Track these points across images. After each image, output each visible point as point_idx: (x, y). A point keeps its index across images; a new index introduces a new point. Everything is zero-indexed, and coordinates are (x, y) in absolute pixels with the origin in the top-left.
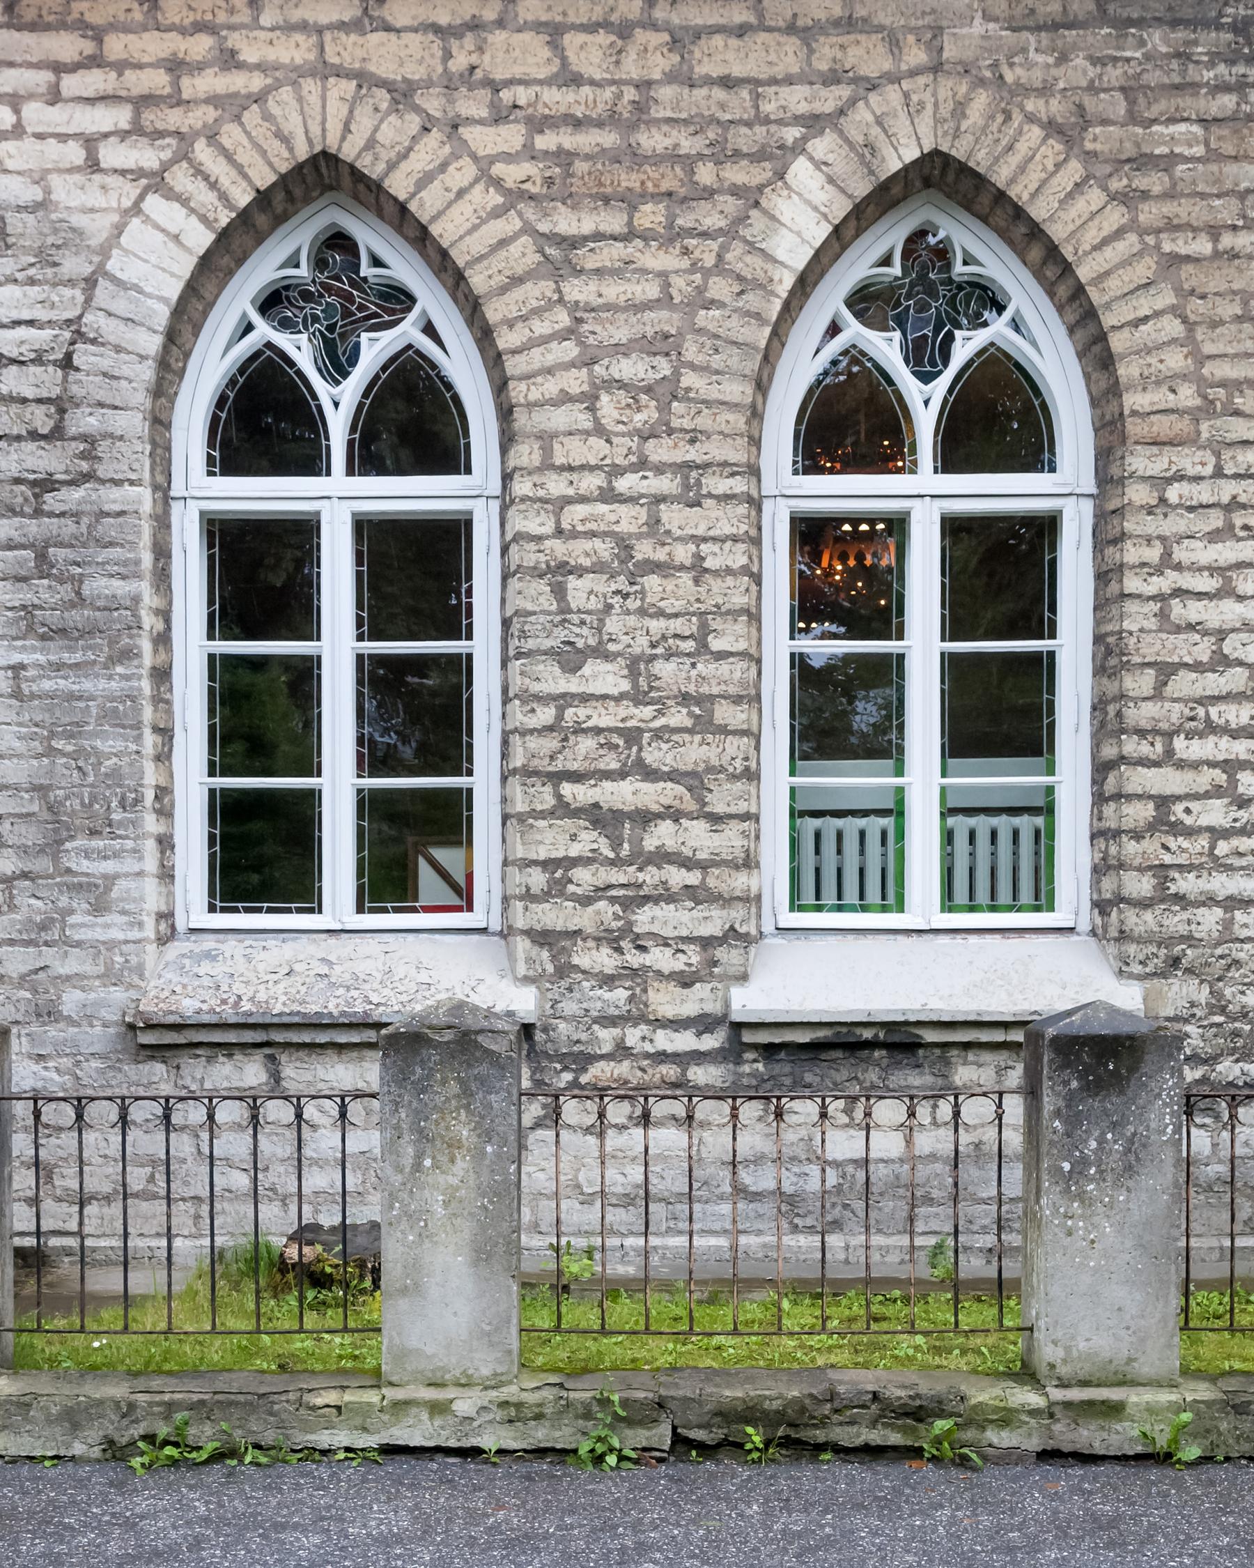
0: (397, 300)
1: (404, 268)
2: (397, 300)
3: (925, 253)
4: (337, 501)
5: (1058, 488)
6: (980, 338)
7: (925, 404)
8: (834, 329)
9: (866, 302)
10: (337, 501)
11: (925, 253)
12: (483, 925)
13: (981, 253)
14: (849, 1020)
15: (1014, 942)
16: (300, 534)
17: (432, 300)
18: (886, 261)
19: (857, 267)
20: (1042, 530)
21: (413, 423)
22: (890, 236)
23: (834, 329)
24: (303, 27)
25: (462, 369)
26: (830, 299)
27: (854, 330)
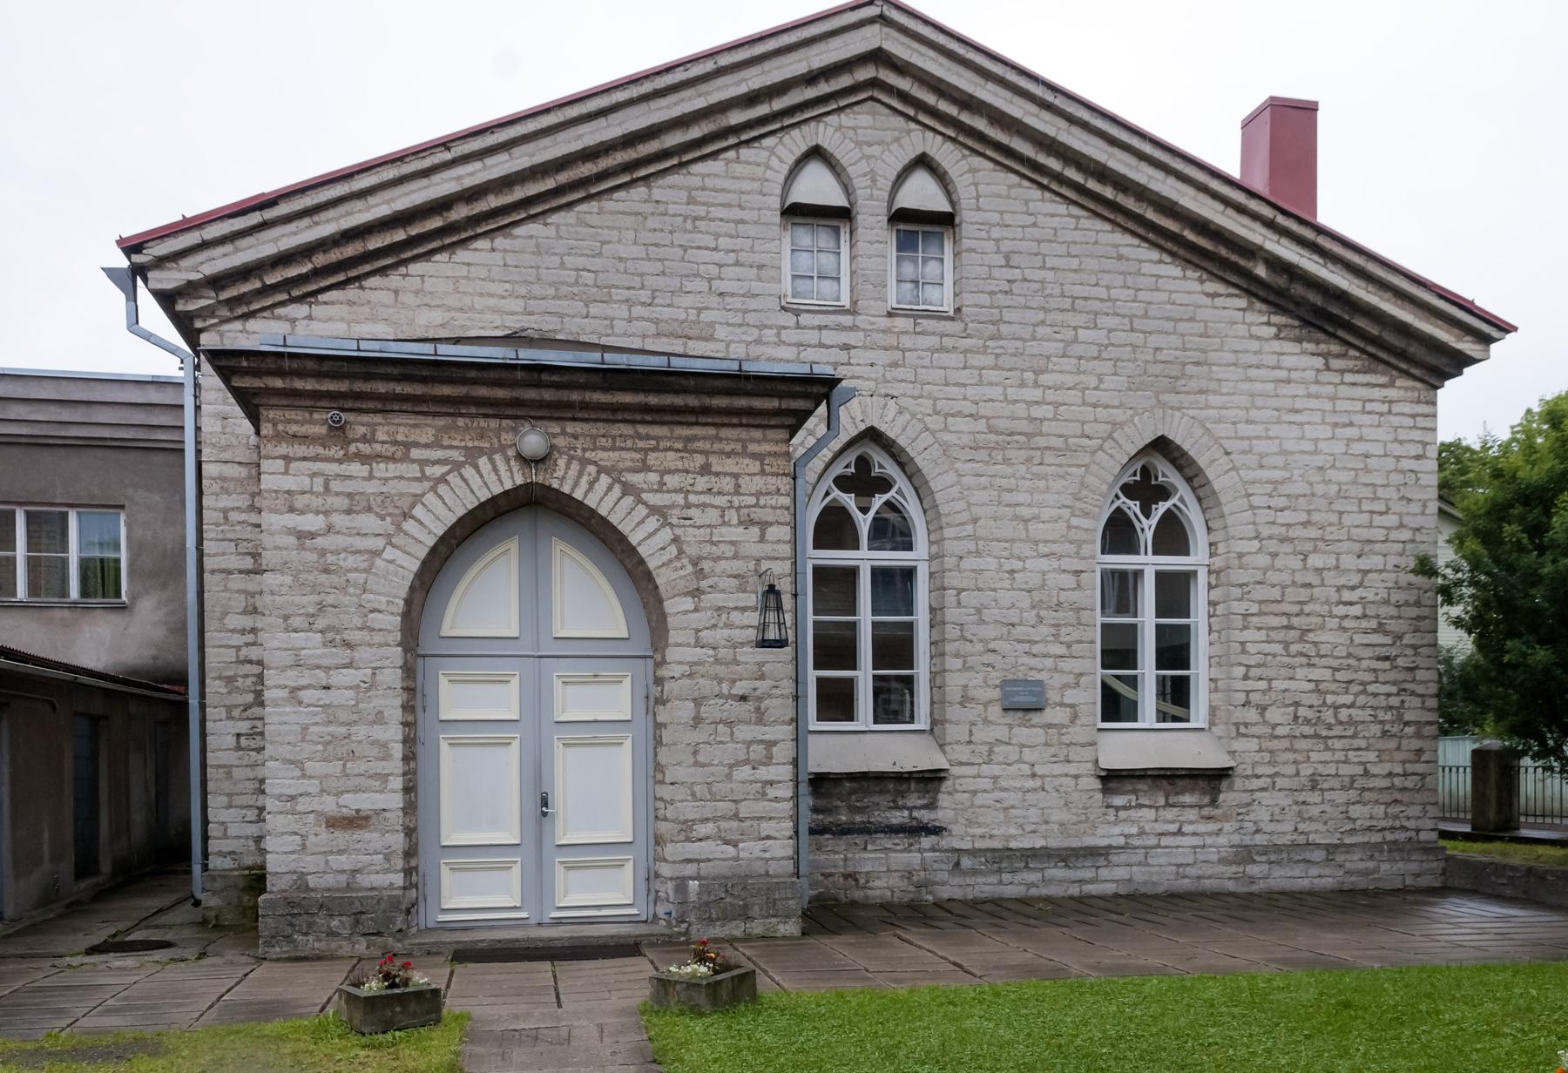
0: (884, 484)
1: (891, 470)
2: (884, 484)
3: (863, 463)
4: (865, 558)
5: (917, 556)
6: (885, 497)
7: (864, 523)
8: (827, 494)
9: (842, 483)
10: (865, 558)
11: (863, 463)
12: (571, 872)
13: (1166, 473)
14: (601, 963)
15: (1115, 734)
16: (851, 574)
17: (901, 482)
18: (1135, 474)
19: (838, 469)
20: (909, 574)
21: (891, 531)
22: (851, 457)
23: (827, 494)
24: (1243, 438)
25: (913, 509)
26: (828, 482)
27: (836, 493)
